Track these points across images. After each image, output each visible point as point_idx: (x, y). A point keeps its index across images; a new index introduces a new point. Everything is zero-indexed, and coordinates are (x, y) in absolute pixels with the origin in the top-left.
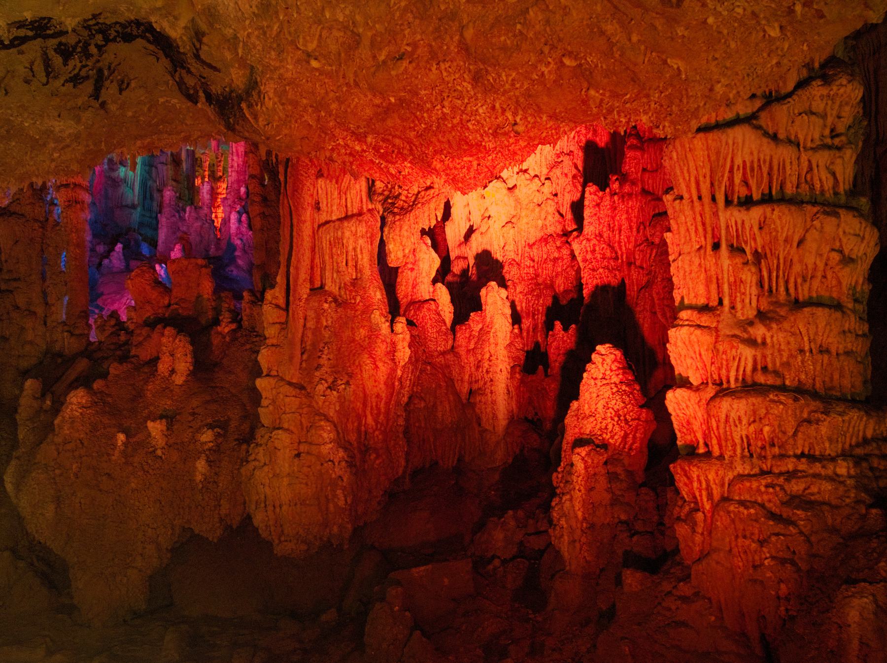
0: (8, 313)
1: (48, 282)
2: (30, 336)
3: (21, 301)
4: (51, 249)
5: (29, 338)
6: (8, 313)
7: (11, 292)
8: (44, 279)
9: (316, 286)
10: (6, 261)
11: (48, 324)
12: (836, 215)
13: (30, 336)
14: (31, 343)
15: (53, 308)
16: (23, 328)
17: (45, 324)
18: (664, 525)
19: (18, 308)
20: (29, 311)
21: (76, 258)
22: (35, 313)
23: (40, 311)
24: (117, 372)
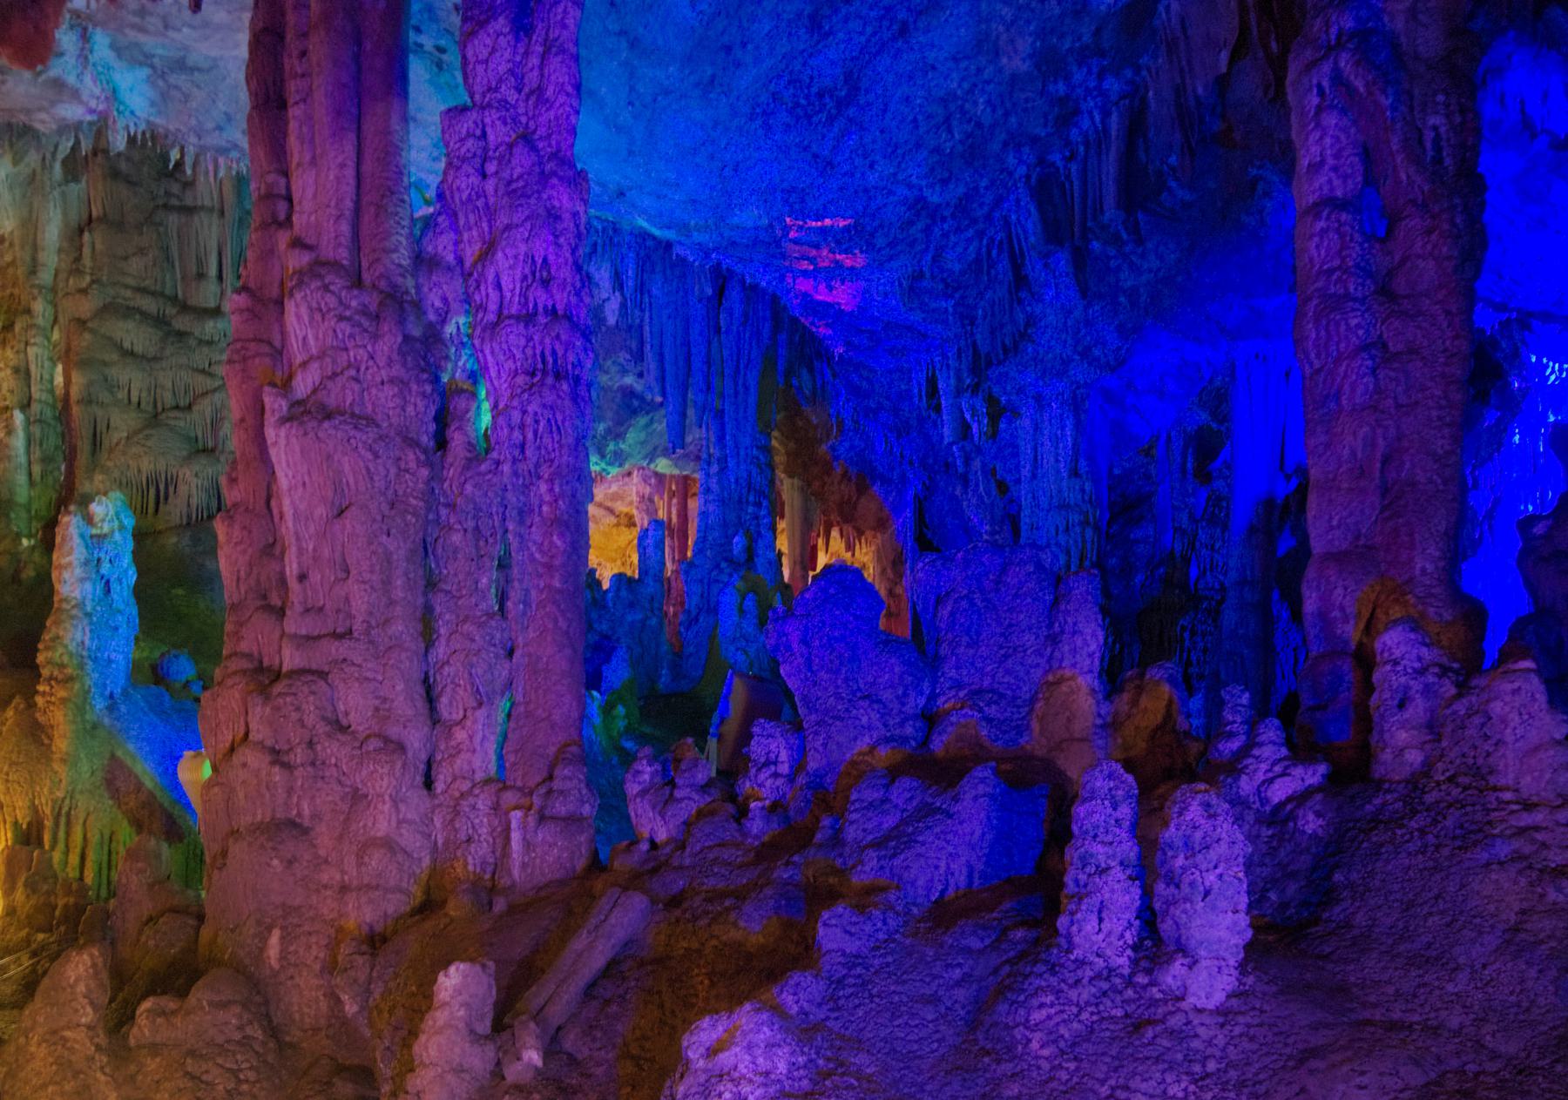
0: (311, 744)
1: (440, 651)
2: (381, 823)
3: (355, 703)
4: (456, 538)
5: (382, 828)
6: (311, 744)
7: (322, 675)
8: (428, 638)
9: (1009, 18)
10: (302, 577)
11: (439, 787)
12: (911, 842)
13: (381, 823)
14: (388, 844)
15: (460, 735)
16: (357, 797)
17: (428, 784)
18: (577, 180)
19: (344, 729)
20: (387, 740)
21: (549, 567)
22: (401, 748)
23: (415, 739)
24: (852, 946)
